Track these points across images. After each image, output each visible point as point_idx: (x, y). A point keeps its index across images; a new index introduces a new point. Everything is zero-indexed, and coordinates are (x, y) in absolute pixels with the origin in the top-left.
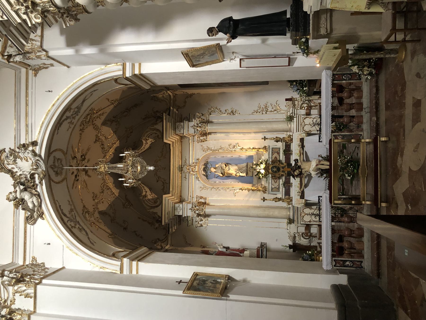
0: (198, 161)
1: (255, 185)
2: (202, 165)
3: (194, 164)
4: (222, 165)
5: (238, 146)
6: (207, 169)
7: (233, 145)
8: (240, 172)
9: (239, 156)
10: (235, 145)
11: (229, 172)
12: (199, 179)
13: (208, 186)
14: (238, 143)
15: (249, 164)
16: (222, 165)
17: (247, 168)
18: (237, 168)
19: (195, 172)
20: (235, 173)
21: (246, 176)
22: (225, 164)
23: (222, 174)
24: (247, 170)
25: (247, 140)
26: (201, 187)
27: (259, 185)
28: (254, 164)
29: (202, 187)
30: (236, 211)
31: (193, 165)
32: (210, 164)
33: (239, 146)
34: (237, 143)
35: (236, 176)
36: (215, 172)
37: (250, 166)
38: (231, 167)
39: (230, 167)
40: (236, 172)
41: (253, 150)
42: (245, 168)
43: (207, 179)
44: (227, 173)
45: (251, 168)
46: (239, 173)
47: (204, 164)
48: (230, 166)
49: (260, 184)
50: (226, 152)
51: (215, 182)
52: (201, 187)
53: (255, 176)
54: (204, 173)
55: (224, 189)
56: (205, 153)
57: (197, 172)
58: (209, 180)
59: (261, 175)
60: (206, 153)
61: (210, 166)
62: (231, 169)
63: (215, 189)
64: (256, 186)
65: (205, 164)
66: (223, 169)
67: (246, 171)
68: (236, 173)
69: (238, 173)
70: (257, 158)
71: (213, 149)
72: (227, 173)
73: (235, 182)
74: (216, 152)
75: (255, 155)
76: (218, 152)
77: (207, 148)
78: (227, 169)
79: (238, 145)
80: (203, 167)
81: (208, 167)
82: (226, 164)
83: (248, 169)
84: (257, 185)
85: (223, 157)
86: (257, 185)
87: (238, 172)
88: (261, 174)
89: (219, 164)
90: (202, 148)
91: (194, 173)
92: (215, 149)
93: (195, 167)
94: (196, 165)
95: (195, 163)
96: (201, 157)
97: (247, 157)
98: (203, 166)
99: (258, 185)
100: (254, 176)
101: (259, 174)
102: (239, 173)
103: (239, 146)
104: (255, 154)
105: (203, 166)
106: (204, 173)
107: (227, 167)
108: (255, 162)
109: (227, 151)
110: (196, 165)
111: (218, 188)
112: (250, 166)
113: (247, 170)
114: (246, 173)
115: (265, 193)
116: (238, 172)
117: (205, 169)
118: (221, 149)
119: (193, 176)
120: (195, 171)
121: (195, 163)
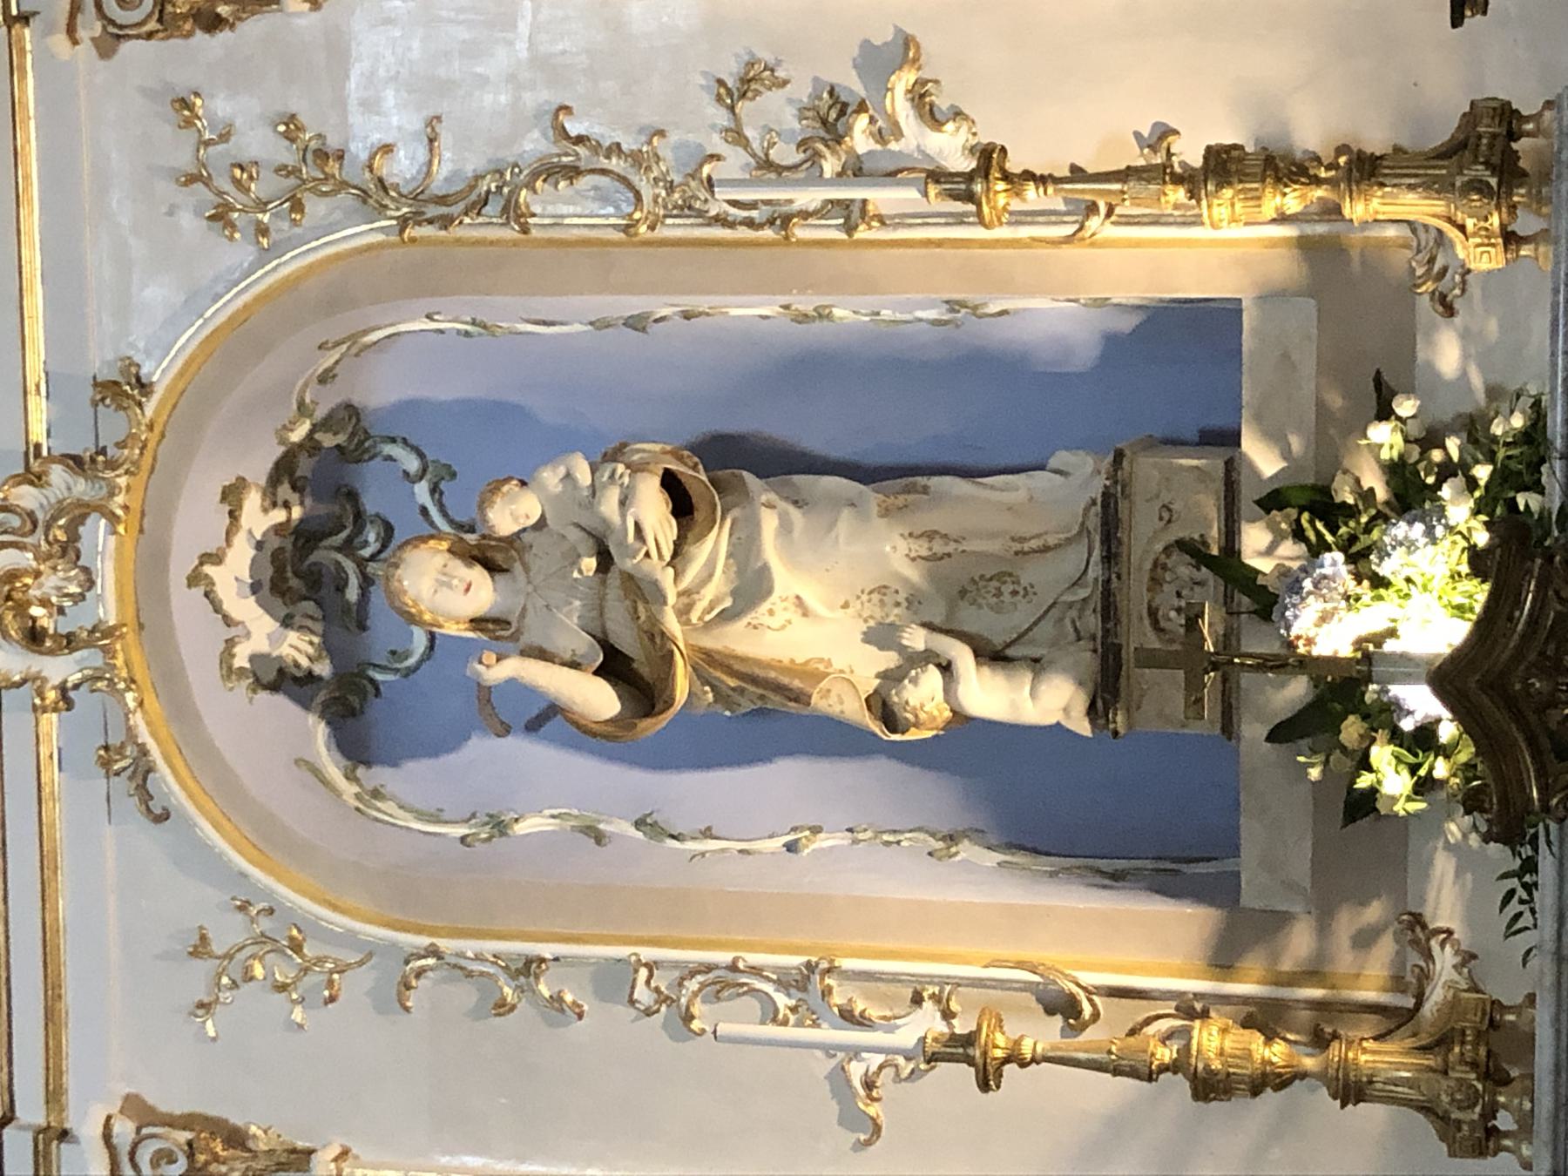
0: (113, 424)
1: (1277, 921)
2: (232, 495)
3: (34, 478)
4: (609, 505)
5: (919, 97)
6: (348, 548)
7: (801, 90)
8: (962, 656)
9: (953, 305)
10: (853, 85)
11: (737, 640)
12: (168, 782)
13: (341, 922)
14: (905, 49)
15: (1147, 469)
16: (609, 505)
17: (1109, 558)
18: (913, 573)
19: (69, 642)
20: (868, 665)
21: (1083, 728)
22: (670, 482)
23: (614, 667)
24: (1109, 608)
25: (414, 332)
26: (201, 948)
27: (1364, 940)
28: (1248, 495)
29: (228, 933)
30: (1189, 911)
31: (26, 497)
32: (412, 464)
33: (942, 103)
34: (882, 35)
35: (890, 719)
36: (477, 623)
37: (1168, 515)
38: (785, 527)
39: (770, 550)
40: (882, 636)
41: (1223, 204)
42: (1071, 561)
43: (334, 772)
44: (710, 657)
45: (1183, 568)
46: (946, 668)
47: (284, 470)
48: (769, 522)
49: (1374, 912)
50: (674, 229)
51: (500, 827)
52: (201, 948)
53: (1282, 733)
54: (297, 648)
55: (643, 995)
56: (240, 251)
57: (101, 635)
58: (379, 775)
59: (1382, 754)
60: (265, 255)
61: (422, 491)
62: (785, 581)
63: (465, 995)
64: (1300, 942)
65: (305, 466)
66: (629, 579)
67: (1093, 622)
68: (890, 659)
69: (933, 676)
70: (1308, 365)
71: (403, 167)
72: (709, 663)
73: (885, 837)
74: (469, 228)
75: (1271, 297)
76: (511, 233)
77: (288, 156)
78: (717, 589)
79: (903, 81)
80: (258, 518)
81: (370, 505)
82: (695, 476)
83: (1135, 595)
84: (1323, 929)
85: (637, 323)
86: (1323, 929)
87: (917, 639)
88: (1396, 736)
89: (551, 478)
90: (184, 159)
91: (59, 669)
92: (437, 186)
93: (69, 550)
94: (79, 513)
95: (57, 474)
96: (189, 339)
97: (1127, 323)
98: (252, 501)
99: (1346, 923)
100: (1253, 731)
101: (1351, 730)
102: (946, 668)
103: (932, 117)
104: (1285, 268)
105: (252, 501)
106: (297, 648)
107: (714, 546)
108: (1275, 437)
109: (686, 208)
110: (79, 513)
111: (529, 967)
112: (1168, 515)
113: (1109, 608)
114: (1087, 659)
115: (1485, 1141)
116: (917, 639)
117: (325, 555)
118: (573, 172)
119: (50, 721)
120: (77, 620)
121: (76, 463)
